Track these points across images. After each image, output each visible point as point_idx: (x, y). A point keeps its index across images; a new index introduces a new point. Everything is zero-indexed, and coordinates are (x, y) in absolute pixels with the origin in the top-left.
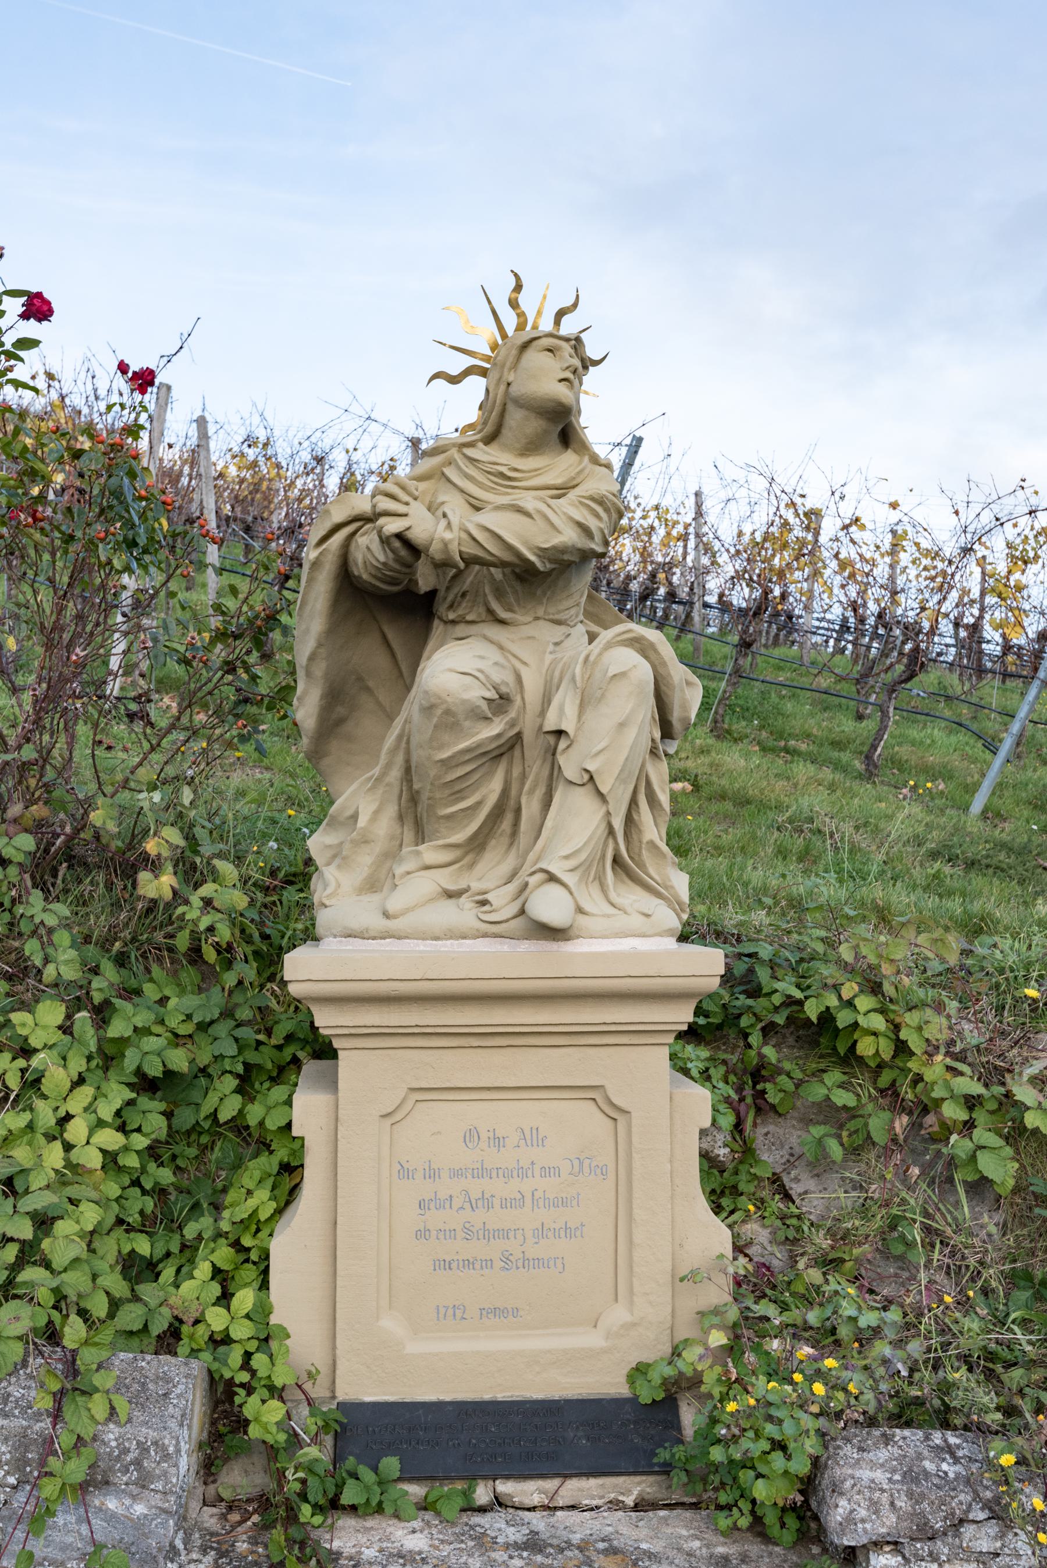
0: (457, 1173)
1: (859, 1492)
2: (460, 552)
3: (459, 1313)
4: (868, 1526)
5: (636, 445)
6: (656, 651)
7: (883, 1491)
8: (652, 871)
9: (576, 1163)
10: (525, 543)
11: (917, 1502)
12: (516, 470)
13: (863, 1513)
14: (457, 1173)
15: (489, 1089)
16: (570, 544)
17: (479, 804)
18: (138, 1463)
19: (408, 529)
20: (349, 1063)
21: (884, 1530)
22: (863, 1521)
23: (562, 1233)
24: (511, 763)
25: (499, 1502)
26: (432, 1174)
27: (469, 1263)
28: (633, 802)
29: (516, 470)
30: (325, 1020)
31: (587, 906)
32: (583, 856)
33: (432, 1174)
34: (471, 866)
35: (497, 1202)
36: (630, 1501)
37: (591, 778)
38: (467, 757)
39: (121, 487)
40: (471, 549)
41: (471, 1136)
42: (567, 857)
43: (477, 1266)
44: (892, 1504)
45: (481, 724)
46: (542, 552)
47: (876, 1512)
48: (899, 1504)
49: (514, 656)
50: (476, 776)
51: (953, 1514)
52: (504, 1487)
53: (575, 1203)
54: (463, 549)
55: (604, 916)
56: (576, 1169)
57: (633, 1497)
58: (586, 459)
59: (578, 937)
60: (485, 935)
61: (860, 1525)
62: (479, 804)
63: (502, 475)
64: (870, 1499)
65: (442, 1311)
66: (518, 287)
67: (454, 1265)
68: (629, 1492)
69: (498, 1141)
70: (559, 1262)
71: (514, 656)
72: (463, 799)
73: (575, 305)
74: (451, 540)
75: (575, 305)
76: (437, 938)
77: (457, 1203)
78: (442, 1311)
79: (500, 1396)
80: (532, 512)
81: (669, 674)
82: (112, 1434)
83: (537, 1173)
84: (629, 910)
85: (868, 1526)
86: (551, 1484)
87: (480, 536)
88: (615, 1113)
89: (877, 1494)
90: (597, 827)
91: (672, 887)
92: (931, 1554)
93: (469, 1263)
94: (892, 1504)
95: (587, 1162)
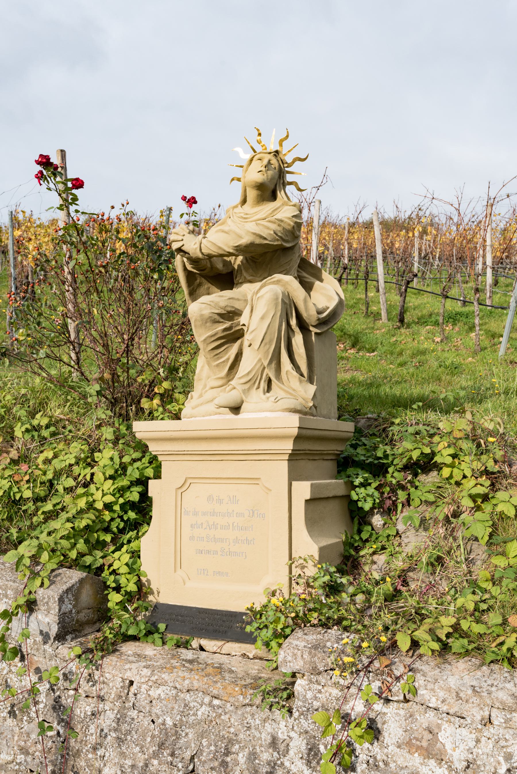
0: (204, 514)
1: (289, 649)
3: (206, 572)
4: (291, 664)
5: (170, 209)
7: (299, 650)
9: (251, 512)
10: (229, 247)
11: (312, 657)
12: (247, 214)
13: (289, 658)
14: (204, 514)
16: (249, 242)
17: (228, 359)
18: (47, 603)
19: (183, 245)
21: (298, 667)
22: (290, 662)
23: (245, 542)
25: (202, 649)
26: (196, 514)
27: (209, 552)
29: (247, 214)
30: (153, 448)
33: (196, 514)
35: (219, 526)
36: (251, 656)
38: (213, 339)
39: (284, 228)
41: (210, 498)
43: (212, 553)
44: (302, 656)
45: (217, 325)
47: (296, 659)
48: (304, 656)
51: (328, 664)
52: (204, 642)
53: (251, 529)
56: (251, 514)
57: (252, 654)
59: (243, 412)
61: (288, 664)
62: (228, 359)
63: (242, 217)
64: (293, 653)
65: (199, 571)
67: (203, 552)
68: (251, 652)
69: (220, 501)
70: (244, 554)
72: (221, 357)
73: (287, 136)
75: (287, 136)
76: (204, 416)
77: (204, 526)
78: (199, 571)
79: (219, 609)
82: (41, 591)
83: (235, 515)
85: (291, 664)
86: (220, 643)
89: (296, 651)
90: (256, 365)
92: (317, 681)
93: (209, 552)
94: (302, 656)
95: (256, 512)
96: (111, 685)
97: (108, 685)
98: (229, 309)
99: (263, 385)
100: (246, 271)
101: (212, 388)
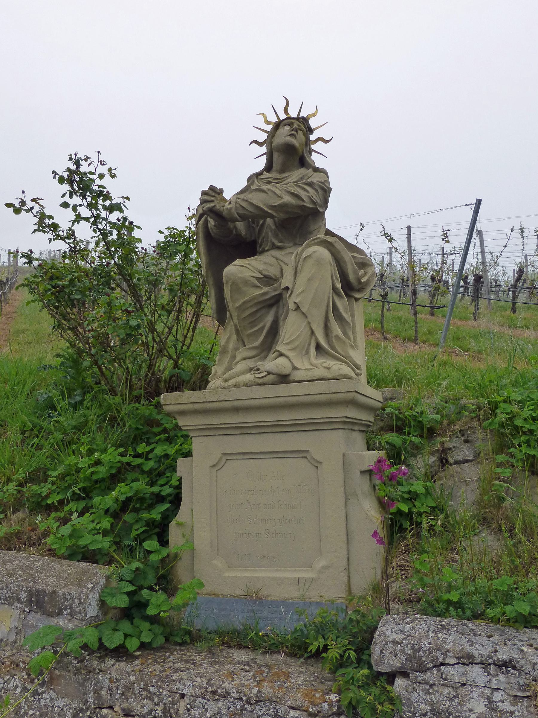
2: (238, 213)
6: (333, 246)
8: (339, 350)
10: (265, 204)
15: (257, 453)
17: (263, 327)
20: (197, 445)
24: (278, 308)
28: (327, 319)
31: (298, 365)
32: (297, 343)
34: (265, 357)
37: (298, 307)
40: (241, 212)
42: (287, 344)
46: (272, 207)
49: (282, 261)
50: (259, 315)
54: (238, 211)
55: (306, 369)
58: (311, 170)
60: (258, 384)
62: (263, 327)
66: (288, 104)
71: (282, 261)
72: (256, 326)
74: (231, 209)
80: (266, 190)
81: (342, 257)
84: (319, 366)
87: (245, 205)
88: (316, 464)
91: (350, 357)
96: (156, 699)
97: (153, 700)
98: (266, 273)
99: (313, 350)
100: (276, 236)
101: (245, 359)
